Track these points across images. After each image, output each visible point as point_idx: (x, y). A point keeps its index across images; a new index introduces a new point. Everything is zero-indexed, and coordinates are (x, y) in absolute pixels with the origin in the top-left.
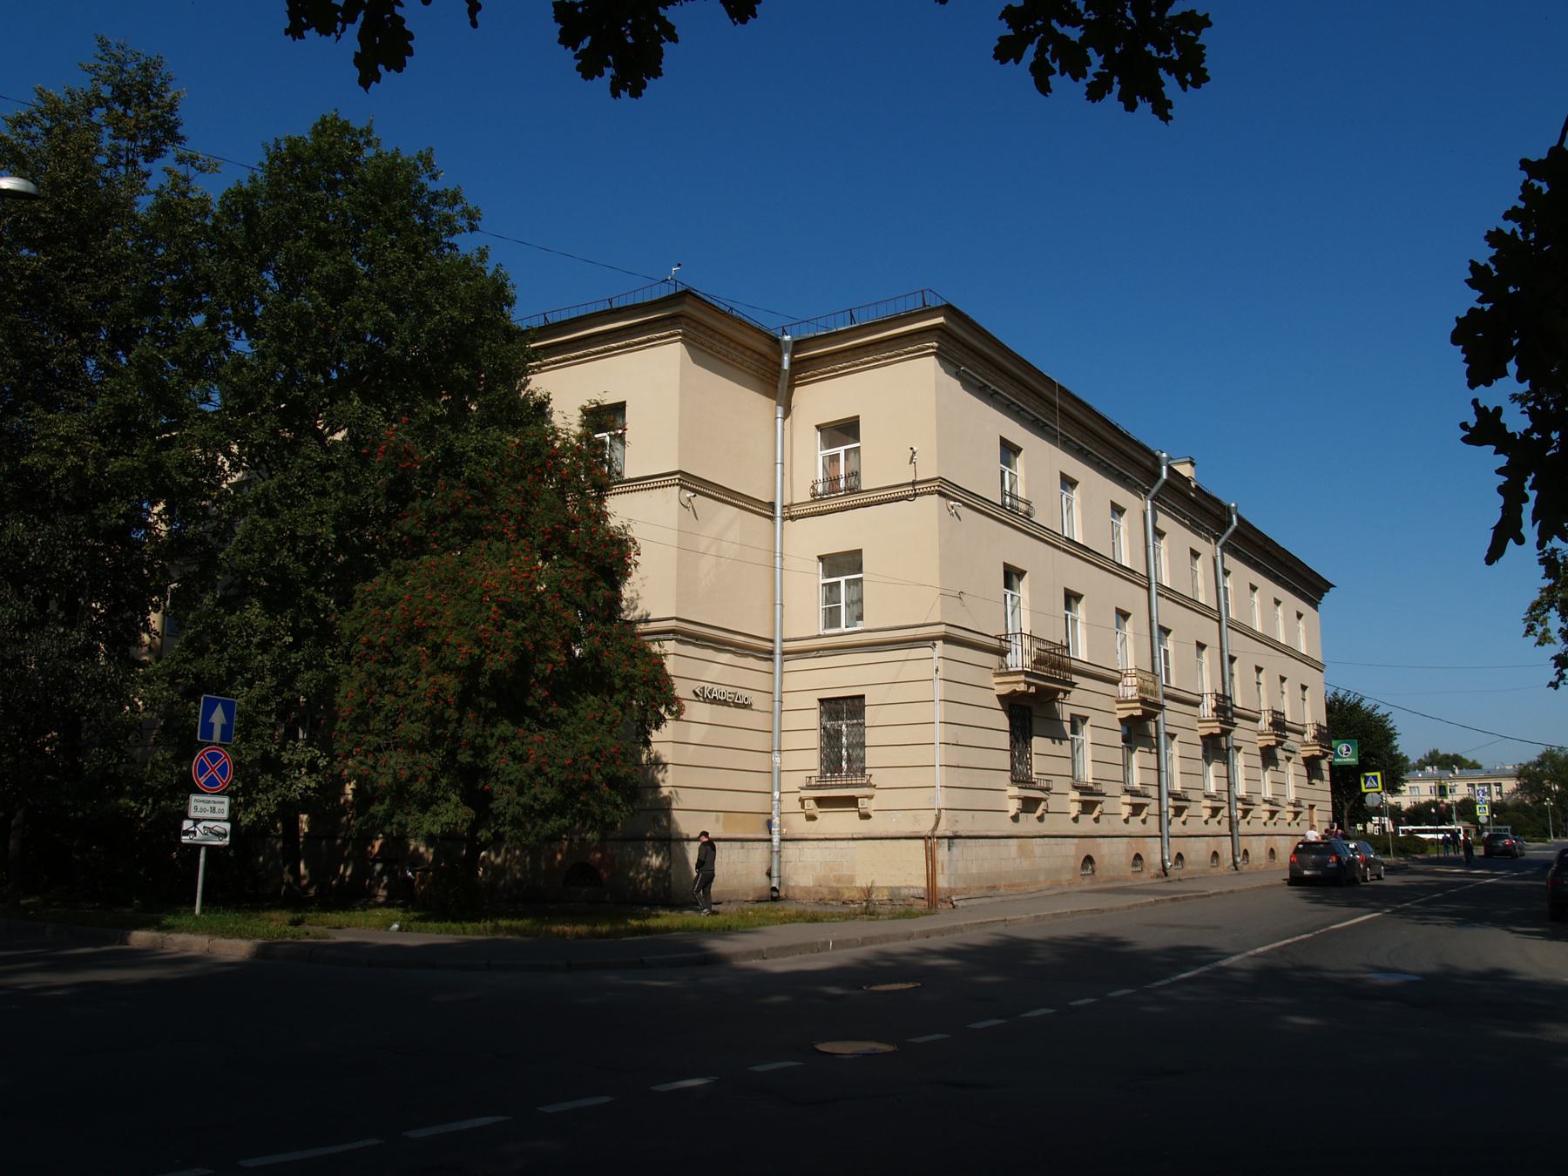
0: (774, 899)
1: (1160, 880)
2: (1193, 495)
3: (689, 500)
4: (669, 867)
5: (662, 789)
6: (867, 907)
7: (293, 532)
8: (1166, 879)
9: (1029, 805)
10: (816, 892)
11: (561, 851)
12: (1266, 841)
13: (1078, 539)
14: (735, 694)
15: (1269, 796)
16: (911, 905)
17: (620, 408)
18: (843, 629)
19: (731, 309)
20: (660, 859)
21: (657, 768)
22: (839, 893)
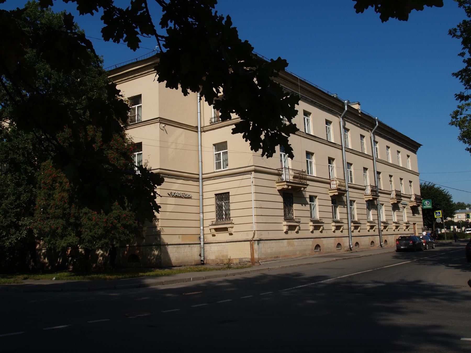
0: (203, 264)
1: (348, 252)
2: (360, 115)
3: (164, 127)
4: (161, 254)
5: (158, 228)
6: (228, 265)
7: (18, 146)
8: (350, 252)
9: (291, 228)
10: (216, 261)
11: (126, 250)
12: (395, 237)
13: (312, 133)
14: (185, 194)
15: (396, 221)
16: (246, 264)
17: (140, 96)
18: (222, 169)
19: (263, 57)
20: (158, 252)
21: (156, 221)
22: (223, 261)
